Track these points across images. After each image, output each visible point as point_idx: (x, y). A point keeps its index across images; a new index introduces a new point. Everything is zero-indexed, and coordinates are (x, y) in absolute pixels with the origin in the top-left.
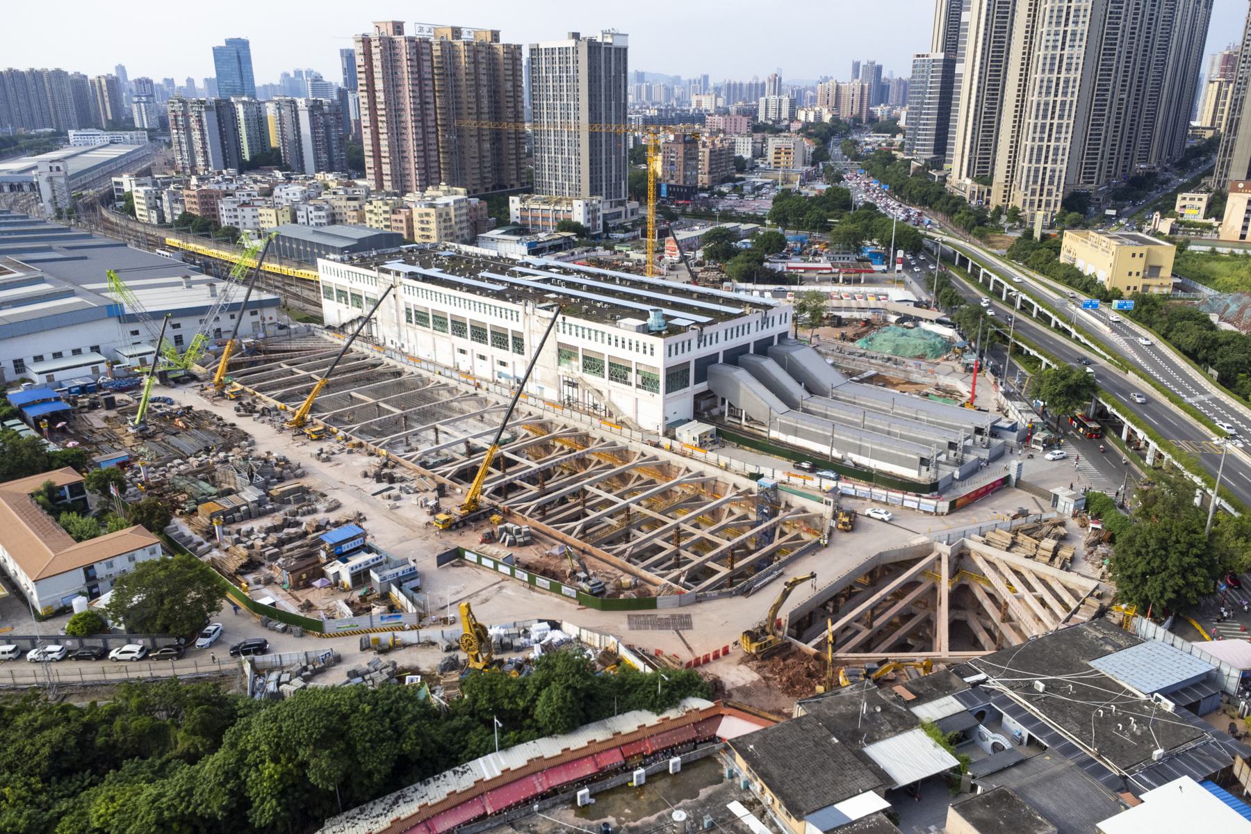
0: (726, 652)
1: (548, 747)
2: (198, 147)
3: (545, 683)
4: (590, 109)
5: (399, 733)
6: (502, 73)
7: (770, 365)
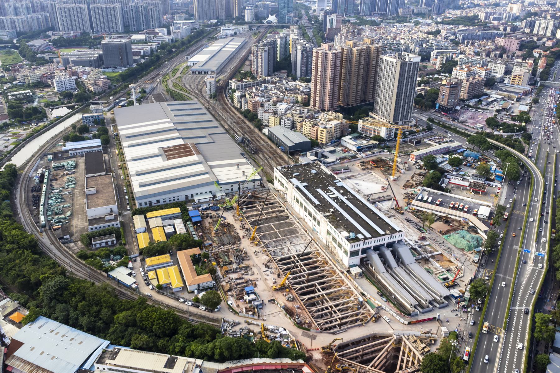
0: (318, 349)
1: (267, 360)
2: (260, 64)
3: (271, 348)
4: (398, 87)
5: (241, 350)
6: (372, 57)
7: (388, 253)
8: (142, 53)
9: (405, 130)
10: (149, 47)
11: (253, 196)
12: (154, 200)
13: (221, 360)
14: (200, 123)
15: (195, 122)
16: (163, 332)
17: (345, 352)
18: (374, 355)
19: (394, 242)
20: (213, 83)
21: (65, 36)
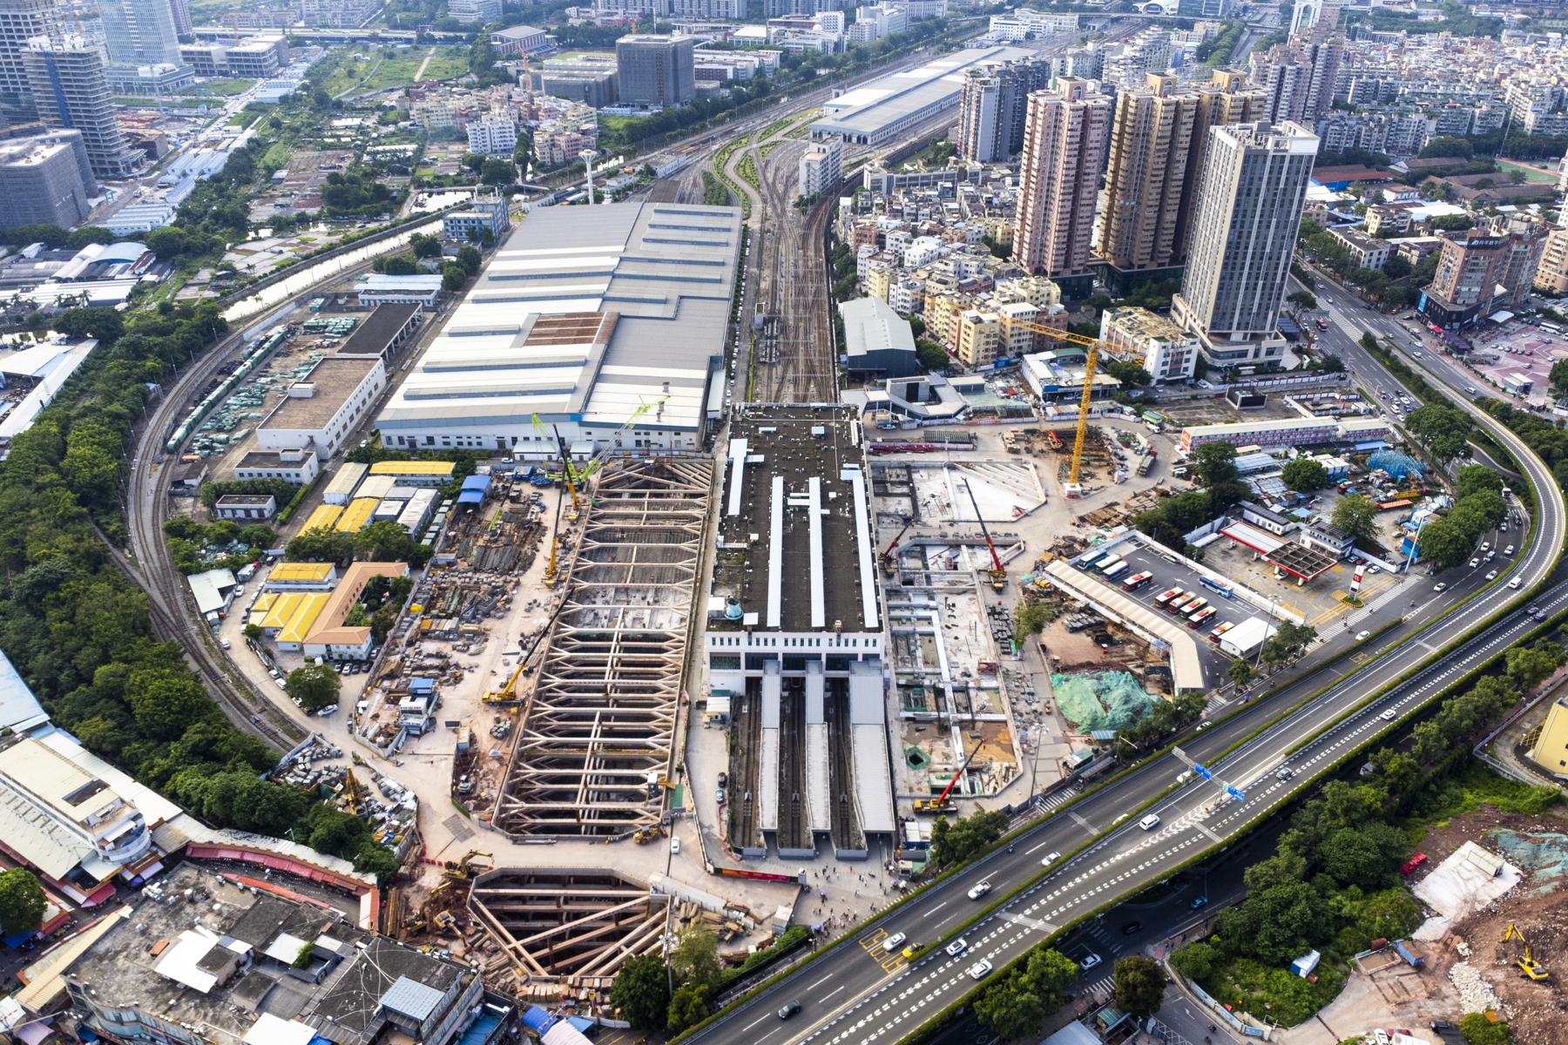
5: (253, 811)
8: (730, 75)
9: (1244, 360)
10: (756, 61)
11: (659, 469)
12: (420, 436)
13: (214, 822)
14: (688, 267)
15: (679, 262)
16: (149, 727)
17: (502, 891)
18: (539, 924)
19: (854, 657)
20: (817, 166)
21: (598, 22)
